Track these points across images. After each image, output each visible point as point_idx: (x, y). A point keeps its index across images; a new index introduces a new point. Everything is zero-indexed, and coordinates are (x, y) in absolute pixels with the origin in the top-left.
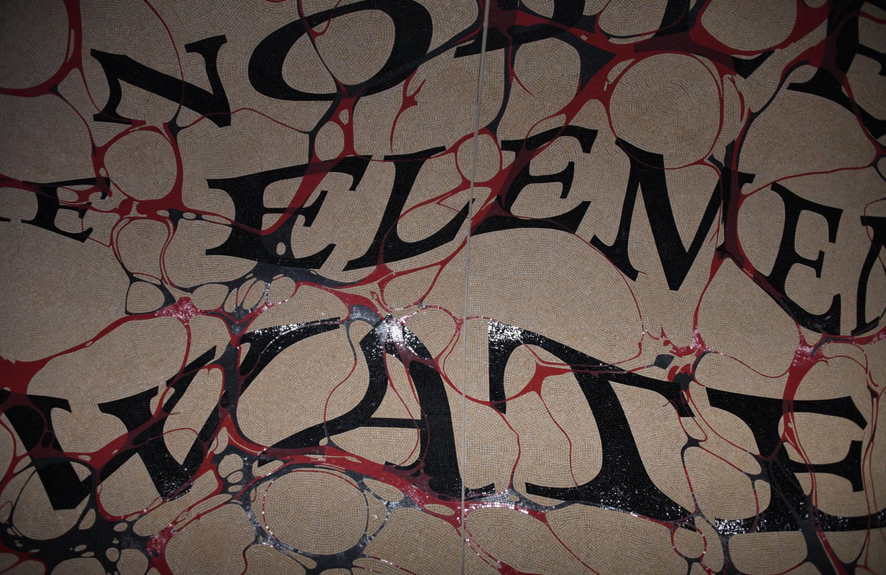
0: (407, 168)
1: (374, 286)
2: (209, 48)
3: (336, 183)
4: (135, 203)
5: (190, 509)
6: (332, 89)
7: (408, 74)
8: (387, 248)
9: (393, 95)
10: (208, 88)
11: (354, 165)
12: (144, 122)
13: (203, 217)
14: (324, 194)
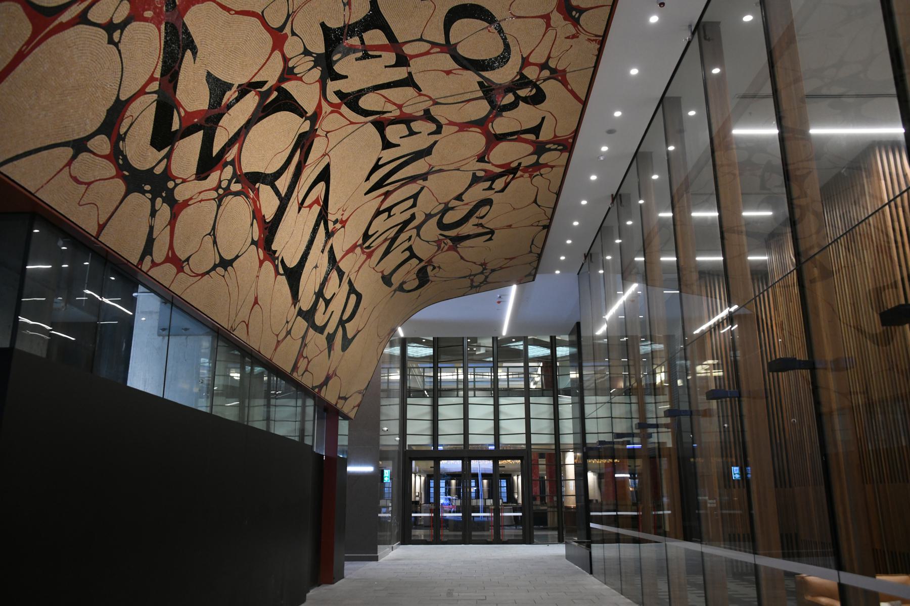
0: (409, 82)
1: (330, 109)
3: (390, 57)
5: (200, 193)
6: (452, 41)
7: (465, 68)
8: (351, 100)
9: (451, 64)
11: (402, 61)
13: (347, 7)
14: (380, 56)
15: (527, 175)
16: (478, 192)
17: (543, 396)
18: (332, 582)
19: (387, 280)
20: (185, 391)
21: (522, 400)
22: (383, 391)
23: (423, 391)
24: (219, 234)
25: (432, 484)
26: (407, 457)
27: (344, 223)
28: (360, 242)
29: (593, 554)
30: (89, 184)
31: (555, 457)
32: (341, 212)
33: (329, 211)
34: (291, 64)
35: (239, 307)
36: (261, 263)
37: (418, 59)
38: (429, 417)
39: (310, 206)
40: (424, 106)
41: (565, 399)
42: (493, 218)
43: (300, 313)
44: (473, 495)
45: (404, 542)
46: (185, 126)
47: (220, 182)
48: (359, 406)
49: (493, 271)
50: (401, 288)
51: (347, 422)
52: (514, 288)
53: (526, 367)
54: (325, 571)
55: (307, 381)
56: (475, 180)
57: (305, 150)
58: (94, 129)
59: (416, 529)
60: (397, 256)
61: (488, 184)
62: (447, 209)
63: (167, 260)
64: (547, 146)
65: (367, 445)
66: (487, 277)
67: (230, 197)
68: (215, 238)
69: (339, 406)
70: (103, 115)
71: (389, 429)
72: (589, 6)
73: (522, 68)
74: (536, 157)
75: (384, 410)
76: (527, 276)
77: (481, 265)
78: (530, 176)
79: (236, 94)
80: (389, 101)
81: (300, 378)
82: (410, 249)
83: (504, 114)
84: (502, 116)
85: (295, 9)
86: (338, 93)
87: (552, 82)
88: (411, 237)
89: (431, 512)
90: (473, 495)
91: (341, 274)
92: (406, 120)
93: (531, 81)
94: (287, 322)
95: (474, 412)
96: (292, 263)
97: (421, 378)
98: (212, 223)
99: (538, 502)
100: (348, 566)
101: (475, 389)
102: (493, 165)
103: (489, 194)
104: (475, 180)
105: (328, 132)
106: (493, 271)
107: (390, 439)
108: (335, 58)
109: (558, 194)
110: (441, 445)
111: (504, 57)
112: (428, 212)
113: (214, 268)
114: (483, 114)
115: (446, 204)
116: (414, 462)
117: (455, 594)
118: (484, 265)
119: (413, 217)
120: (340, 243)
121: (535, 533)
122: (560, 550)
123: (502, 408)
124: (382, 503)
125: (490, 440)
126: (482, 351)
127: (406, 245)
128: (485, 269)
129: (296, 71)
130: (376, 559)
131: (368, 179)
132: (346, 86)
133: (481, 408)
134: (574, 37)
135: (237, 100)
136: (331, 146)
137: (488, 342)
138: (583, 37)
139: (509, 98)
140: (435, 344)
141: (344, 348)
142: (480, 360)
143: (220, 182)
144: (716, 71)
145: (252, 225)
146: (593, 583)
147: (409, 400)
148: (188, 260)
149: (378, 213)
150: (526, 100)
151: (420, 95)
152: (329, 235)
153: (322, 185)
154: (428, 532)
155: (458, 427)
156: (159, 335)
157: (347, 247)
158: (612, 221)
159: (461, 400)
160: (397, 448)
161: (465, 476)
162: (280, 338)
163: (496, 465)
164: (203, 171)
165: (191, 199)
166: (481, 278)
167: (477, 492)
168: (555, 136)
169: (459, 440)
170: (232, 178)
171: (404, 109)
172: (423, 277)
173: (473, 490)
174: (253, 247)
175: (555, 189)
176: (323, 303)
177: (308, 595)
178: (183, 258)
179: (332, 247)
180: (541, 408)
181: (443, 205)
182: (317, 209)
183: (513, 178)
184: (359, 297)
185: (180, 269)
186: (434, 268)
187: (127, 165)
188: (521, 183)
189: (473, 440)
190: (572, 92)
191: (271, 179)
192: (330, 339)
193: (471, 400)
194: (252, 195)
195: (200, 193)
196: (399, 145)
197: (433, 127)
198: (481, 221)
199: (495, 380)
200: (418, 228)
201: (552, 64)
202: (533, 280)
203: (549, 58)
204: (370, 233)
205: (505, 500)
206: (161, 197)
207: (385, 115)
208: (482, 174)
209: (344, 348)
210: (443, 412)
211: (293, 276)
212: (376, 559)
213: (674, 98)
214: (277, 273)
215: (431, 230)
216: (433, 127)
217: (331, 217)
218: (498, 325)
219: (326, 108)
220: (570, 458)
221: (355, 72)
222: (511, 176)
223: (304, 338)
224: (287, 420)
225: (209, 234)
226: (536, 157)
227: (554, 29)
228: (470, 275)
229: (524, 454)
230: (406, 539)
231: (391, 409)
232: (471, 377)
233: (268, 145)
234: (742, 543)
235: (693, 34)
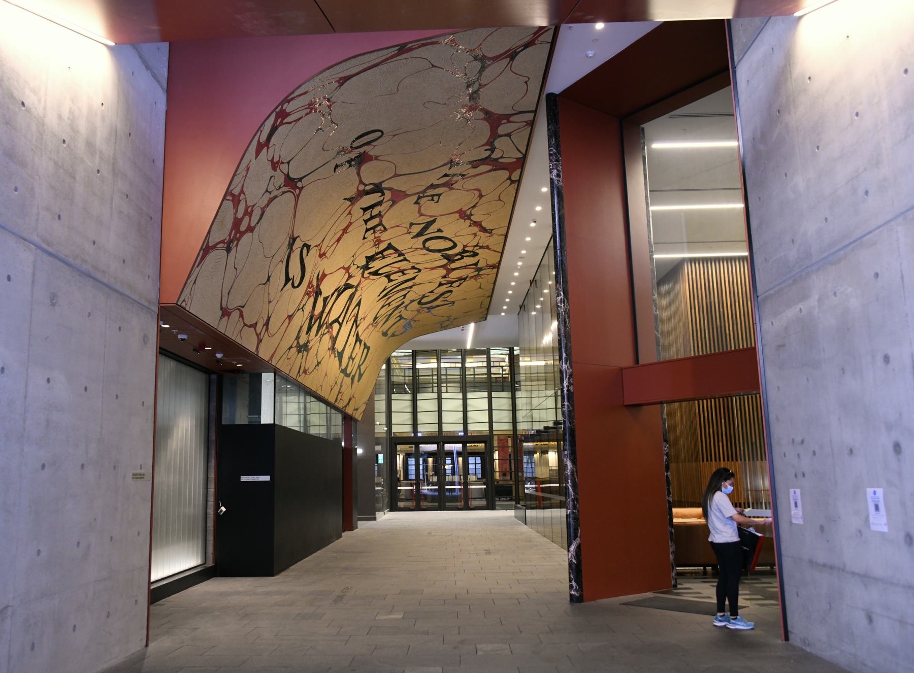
0: (405, 259)
2: (439, 230)
16: (444, 288)
19: (385, 334)
26: (393, 442)
27: (364, 318)
38: (410, 410)
42: (451, 297)
45: (391, 510)
50: (393, 335)
52: (472, 326)
54: (349, 525)
55: (340, 405)
56: (441, 284)
62: (424, 296)
82: (400, 316)
92: (403, 272)
95: (446, 405)
101: (447, 382)
104: (441, 284)
107: (380, 428)
109: (495, 284)
122: (511, 513)
123: (469, 402)
125: (460, 428)
130: (375, 519)
146: (525, 528)
147: (394, 396)
149: (383, 306)
152: (357, 327)
155: (434, 418)
159: (435, 396)
160: (384, 435)
161: (440, 456)
163: (464, 446)
167: (453, 469)
169: (435, 428)
173: (448, 467)
189: (446, 428)
193: (444, 395)
200: (406, 307)
211: (340, 355)
212: (375, 519)
218: (465, 342)
230: (393, 508)
232: (443, 365)
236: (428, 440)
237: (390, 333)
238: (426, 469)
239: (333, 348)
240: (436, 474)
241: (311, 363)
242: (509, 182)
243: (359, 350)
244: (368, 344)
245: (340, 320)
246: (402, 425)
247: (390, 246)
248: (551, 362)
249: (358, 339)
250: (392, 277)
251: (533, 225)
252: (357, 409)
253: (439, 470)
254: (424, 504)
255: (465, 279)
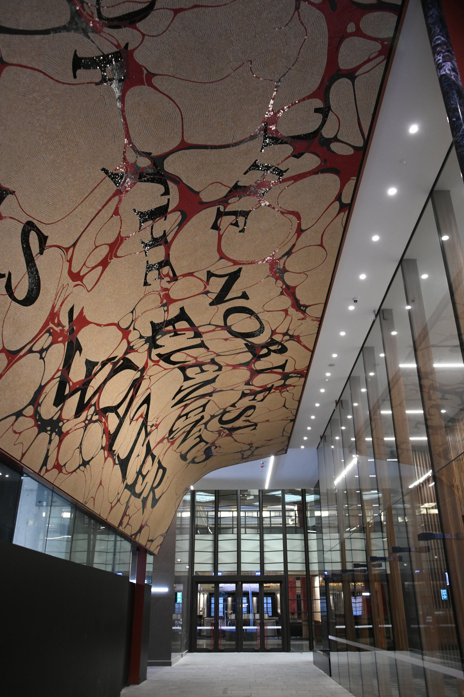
0: (202, 345)
2: (245, 296)
4: (167, 292)
5: (76, 425)
6: (229, 324)
8: (166, 358)
9: (229, 336)
10: (227, 278)
11: (198, 335)
12: (208, 285)
14: (185, 334)
15: (278, 391)
16: (246, 402)
17: (296, 533)
18: (137, 681)
19: (183, 457)
20: (55, 545)
21: (281, 536)
22: (178, 528)
23: (206, 528)
24: (83, 447)
25: (213, 601)
26: (195, 581)
27: (157, 426)
28: (167, 435)
29: (331, 660)
30: (20, 433)
31: (307, 579)
32: (156, 419)
33: (149, 420)
34: (131, 345)
35: (90, 489)
36: (106, 459)
37: (207, 334)
38: (211, 549)
39: (137, 420)
40: (211, 357)
41: (313, 536)
42: (255, 416)
43: (127, 487)
44: (245, 610)
45: (190, 651)
46: (71, 391)
47: (87, 416)
48: (161, 545)
49: (257, 448)
50: (193, 461)
51: (152, 557)
52: (272, 459)
53: (284, 511)
54: (134, 675)
55: (128, 531)
56: (244, 395)
57: (136, 388)
58: (27, 403)
59: (200, 639)
60: (191, 441)
61: (252, 397)
62: (225, 412)
63: (54, 467)
64: (290, 375)
65: (166, 573)
66: (253, 452)
67: (92, 424)
68: (81, 449)
69: (148, 547)
70: (32, 395)
71: (182, 558)
72: (311, 304)
73: (271, 336)
74: (283, 381)
75: (178, 544)
76: (281, 450)
77: (249, 445)
78: (280, 392)
79: (100, 366)
80: (189, 356)
81: (123, 530)
82: (200, 436)
83: (261, 359)
84: (260, 360)
85: (137, 317)
86: (159, 355)
87: (291, 342)
88: (200, 430)
89: (212, 626)
90: (245, 610)
91: (153, 457)
92: (200, 365)
93: (278, 342)
94: (118, 494)
95: (245, 546)
96: (123, 456)
97: (205, 517)
98: (80, 441)
99: (296, 616)
100: (150, 670)
101: (246, 528)
102: (255, 386)
103: (253, 403)
104: (244, 395)
105: (150, 376)
106: (257, 448)
107: (182, 567)
108: (157, 338)
109: (300, 401)
110: (220, 572)
111: (261, 331)
112: (212, 414)
113: (78, 468)
114: (248, 360)
115: (225, 409)
116: (199, 585)
117: (229, 692)
118: (251, 444)
119: (202, 418)
120: (153, 439)
121: (291, 643)
123: (266, 543)
124: (174, 616)
125: (258, 568)
126: (252, 497)
127: (198, 434)
128: (251, 447)
129: (134, 348)
130: (170, 664)
131: (174, 398)
132: (162, 351)
133: (250, 543)
134: (303, 319)
135: (100, 369)
136: (151, 384)
137: (256, 492)
138: (308, 319)
139: (265, 351)
140: (217, 493)
141: (153, 506)
142: (250, 504)
143: (87, 416)
144: (372, 374)
145: (102, 438)
146: (331, 684)
147: (197, 536)
148: (65, 465)
149: (180, 417)
150: (275, 351)
151: (208, 351)
152: (147, 434)
153: (145, 406)
154: (209, 641)
156: (36, 505)
157: (158, 439)
158: (376, 340)
159: (235, 536)
161: (238, 595)
162: (113, 505)
163: (261, 586)
164: (78, 414)
165: (71, 429)
166: (249, 453)
167: (248, 607)
168: (295, 370)
170: (94, 413)
171: (198, 359)
172: (208, 453)
173: (245, 606)
174: (102, 450)
175: (297, 398)
176: (142, 478)
177: (122, 692)
178: (62, 465)
179: (149, 442)
180: (295, 542)
181: (222, 410)
182: (141, 420)
183: (269, 393)
184: (165, 470)
185: (60, 471)
186: (216, 447)
187: (41, 419)
188: (274, 396)
189: (244, 568)
190: (304, 346)
191: (114, 409)
192: (144, 501)
193: (243, 536)
194: (104, 420)
195: (76, 425)
196: (194, 378)
197: (217, 368)
198: (248, 418)
199: (261, 519)
200: (206, 424)
201: (290, 333)
202: (286, 453)
203: (288, 330)
204: (174, 429)
205: (270, 614)
206: (55, 432)
207: (187, 363)
208: (248, 392)
209: (153, 506)
210: (222, 545)
211: (124, 464)
212: (170, 664)
213: (369, 347)
214: (115, 464)
215: (215, 425)
216: (217, 368)
217: (149, 424)
218: (262, 482)
219: (150, 363)
220: (317, 582)
221: (167, 343)
222: (267, 392)
223: (128, 502)
224: (111, 556)
225: (78, 448)
226: (283, 381)
227: (290, 316)
228: (242, 451)
229: (283, 579)
230: (193, 648)
231: (183, 543)
232: (242, 514)
233: (115, 390)
234: (448, 651)
235: (376, 316)
236: (227, 579)
237: (190, 457)
238: (226, 607)
239: (109, 448)
240: (234, 612)
241: (68, 454)
242: (337, 204)
243: (150, 467)
244: (164, 464)
245: (121, 411)
246: (203, 565)
247: (183, 315)
248: (335, 513)
249: (149, 451)
250: (189, 372)
251: (351, 308)
252: (152, 541)
253: (236, 608)
254: (223, 642)
255: (269, 389)
